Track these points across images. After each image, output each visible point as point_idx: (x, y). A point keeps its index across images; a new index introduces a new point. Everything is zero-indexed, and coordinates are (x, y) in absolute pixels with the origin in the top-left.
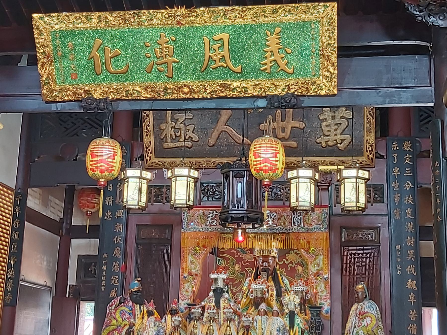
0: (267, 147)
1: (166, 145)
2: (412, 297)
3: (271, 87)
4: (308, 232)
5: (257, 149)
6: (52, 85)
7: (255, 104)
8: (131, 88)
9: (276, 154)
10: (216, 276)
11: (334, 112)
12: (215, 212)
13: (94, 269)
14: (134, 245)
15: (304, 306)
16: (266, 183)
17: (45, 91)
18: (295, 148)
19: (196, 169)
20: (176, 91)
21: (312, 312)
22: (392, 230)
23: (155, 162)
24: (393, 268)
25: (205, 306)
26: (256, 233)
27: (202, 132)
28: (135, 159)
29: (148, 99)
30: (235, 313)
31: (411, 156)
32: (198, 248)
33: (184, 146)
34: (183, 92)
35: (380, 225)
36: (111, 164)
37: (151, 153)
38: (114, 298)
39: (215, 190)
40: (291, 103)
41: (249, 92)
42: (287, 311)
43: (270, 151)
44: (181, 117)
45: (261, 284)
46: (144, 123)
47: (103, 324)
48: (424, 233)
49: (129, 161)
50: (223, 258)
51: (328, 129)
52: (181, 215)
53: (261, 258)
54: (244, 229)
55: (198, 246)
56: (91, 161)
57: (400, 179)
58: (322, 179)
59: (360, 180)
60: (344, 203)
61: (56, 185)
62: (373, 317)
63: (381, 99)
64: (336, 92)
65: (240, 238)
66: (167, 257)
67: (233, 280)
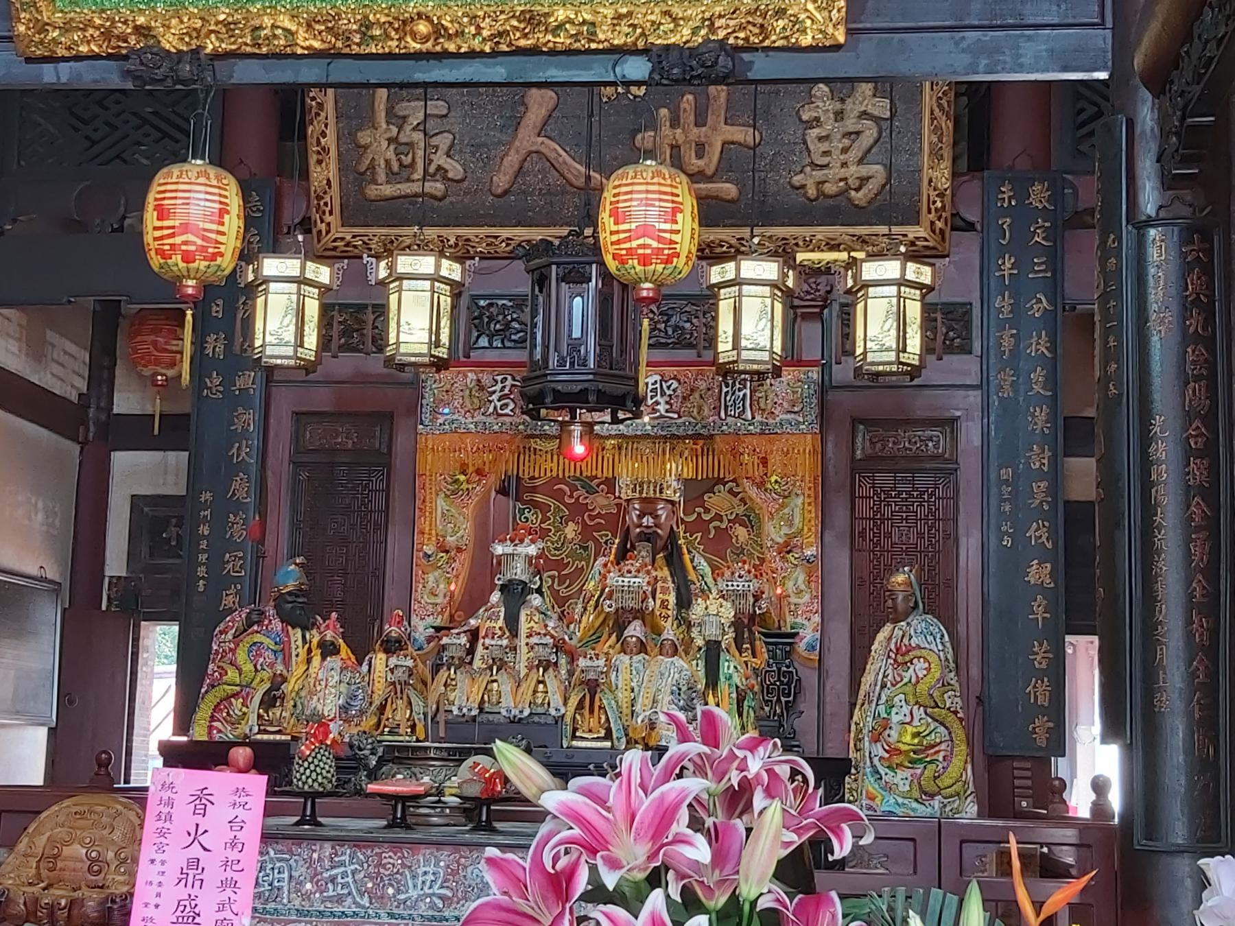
0: (648, 192)
1: (372, 191)
2: (1039, 610)
3: (660, 24)
4: (762, 433)
5: (622, 198)
6: (43, 9)
7: (618, 69)
8: (267, 22)
9: (675, 211)
10: (509, 550)
11: (842, 100)
12: (509, 378)
13: (178, 534)
14: (286, 469)
15: (750, 631)
16: (645, 294)
17: (22, 28)
18: (732, 201)
19: (460, 259)
20: (396, 30)
21: (771, 648)
22: (992, 427)
23: (343, 239)
24: (992, 527)
25: (478, 628)
26: (622, 436)
27: (473, 154)
28: (285, 230)
29: (315, 54)
30: (559, 646)
31: (1047, 224)
32: (462, 478)
33: (423, 194)
34: (414, 36)
35: (958, 413)
36: (213, 236)
37: (331, 213)
38: (231, 611)
39: (509, 318)
40: (718, 68)
41: (601, 36)
42: (700, 642)
43: (657, 203)
44: (414, 111)
45: (634, 573)
46: (310, 129)
47: (204, 680)
48: (1074, 435)
49: (268, 229)
50: (535, 505)
51: (824, 147)
52: (416, 386)
53: (637, 506)
54: (589, 426)
55: (464, 473)
56: (155, 229)
57: (1017, 288)
58: (806, 287)
59: (908, 290)
60: (865, 353)
61: (65, 300)
62: (933, 658)
63: (967, 59)
64: (841, 39)
65: (579, 449)
66: (378, 501)
67: (559, 565)
